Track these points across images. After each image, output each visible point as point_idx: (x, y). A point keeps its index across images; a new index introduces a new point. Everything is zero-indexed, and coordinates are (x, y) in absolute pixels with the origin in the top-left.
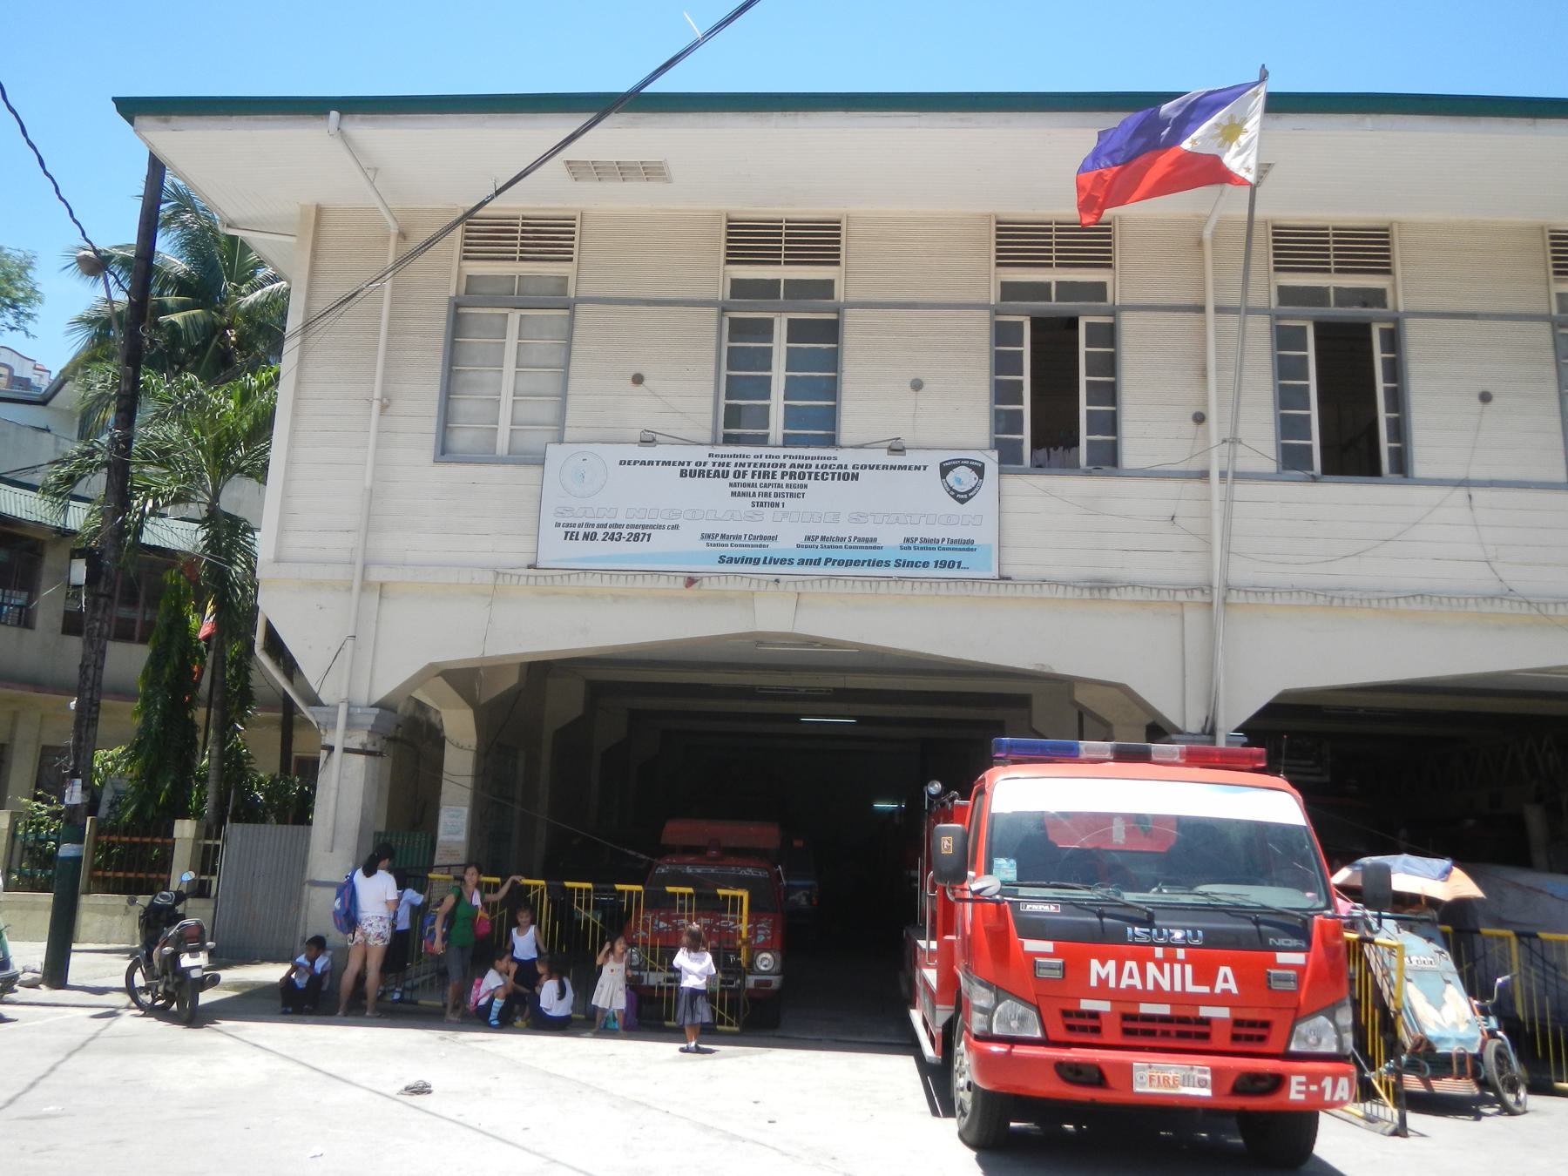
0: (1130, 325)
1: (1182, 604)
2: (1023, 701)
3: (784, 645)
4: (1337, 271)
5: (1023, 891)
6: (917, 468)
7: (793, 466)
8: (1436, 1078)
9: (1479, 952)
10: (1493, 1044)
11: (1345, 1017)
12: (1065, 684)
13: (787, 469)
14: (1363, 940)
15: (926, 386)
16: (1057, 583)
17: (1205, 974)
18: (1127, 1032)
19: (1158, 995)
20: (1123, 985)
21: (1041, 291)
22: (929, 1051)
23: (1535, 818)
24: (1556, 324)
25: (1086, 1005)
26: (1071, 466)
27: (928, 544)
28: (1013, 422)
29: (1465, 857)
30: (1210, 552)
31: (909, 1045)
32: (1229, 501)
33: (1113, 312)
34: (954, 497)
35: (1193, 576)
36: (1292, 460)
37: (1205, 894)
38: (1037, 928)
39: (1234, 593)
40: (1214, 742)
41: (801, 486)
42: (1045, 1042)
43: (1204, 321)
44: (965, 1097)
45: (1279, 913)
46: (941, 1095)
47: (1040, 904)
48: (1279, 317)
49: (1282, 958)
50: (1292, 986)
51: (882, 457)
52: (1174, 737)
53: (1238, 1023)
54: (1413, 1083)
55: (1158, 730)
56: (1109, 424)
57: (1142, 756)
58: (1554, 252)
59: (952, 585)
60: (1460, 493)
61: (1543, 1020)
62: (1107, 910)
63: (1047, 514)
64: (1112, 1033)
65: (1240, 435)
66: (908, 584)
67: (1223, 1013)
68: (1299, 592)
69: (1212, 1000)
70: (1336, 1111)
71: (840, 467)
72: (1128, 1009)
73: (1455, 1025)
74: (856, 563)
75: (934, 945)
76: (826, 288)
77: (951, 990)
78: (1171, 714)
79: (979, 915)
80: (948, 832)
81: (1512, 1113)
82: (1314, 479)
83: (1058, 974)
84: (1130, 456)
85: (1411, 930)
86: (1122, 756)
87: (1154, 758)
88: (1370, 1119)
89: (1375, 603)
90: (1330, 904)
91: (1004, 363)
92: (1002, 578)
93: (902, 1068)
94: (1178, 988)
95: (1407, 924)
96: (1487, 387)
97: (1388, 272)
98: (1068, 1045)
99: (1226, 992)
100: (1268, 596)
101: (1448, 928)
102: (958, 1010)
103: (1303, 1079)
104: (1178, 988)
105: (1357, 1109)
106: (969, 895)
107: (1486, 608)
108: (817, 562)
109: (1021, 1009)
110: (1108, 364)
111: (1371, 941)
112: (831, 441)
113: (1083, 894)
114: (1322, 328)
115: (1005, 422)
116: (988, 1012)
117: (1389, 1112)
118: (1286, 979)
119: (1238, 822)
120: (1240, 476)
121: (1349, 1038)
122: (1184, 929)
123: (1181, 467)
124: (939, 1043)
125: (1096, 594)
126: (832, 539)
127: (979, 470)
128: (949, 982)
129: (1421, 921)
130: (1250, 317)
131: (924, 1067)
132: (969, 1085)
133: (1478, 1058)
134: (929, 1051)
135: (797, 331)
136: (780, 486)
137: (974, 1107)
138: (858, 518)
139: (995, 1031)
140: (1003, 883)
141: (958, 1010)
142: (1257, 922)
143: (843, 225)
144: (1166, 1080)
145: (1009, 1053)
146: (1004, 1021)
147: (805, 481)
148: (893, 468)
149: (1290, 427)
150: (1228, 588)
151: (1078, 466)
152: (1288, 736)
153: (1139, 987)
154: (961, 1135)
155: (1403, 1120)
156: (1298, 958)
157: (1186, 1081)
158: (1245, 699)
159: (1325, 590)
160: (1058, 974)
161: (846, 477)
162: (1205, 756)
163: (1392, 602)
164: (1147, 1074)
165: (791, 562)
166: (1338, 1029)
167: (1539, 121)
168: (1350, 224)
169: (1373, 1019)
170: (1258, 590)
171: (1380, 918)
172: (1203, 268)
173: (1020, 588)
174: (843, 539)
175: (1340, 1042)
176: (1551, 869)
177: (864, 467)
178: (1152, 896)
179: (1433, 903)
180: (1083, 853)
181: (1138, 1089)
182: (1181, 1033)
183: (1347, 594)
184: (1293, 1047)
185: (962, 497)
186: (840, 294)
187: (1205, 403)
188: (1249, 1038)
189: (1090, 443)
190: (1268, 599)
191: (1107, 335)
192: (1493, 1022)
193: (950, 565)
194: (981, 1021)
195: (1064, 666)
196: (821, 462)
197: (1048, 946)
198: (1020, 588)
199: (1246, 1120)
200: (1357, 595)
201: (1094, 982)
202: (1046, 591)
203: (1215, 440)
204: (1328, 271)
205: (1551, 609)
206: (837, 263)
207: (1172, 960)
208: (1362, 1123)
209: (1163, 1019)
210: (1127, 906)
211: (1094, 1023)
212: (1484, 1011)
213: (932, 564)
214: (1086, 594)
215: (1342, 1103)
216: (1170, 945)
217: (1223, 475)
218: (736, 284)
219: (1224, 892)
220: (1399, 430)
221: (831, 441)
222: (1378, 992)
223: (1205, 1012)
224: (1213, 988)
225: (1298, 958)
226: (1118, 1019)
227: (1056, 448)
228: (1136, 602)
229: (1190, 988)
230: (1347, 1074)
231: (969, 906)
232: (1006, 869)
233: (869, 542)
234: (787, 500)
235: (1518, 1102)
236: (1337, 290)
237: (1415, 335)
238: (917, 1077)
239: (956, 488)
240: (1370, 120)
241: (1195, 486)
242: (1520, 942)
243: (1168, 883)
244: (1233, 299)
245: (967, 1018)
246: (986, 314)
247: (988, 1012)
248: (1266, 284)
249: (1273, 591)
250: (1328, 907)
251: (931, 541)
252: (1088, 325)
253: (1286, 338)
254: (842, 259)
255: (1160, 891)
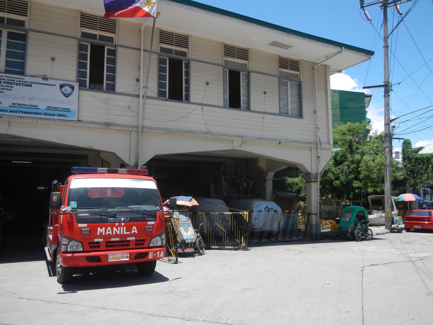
0: (120, 51)
1: (131, 131)
2: (85, 157)
3: (9, 138)
4: (175, 45)
5: (79, 210)
6: (52, 85)
7: (8, 80)
8: (185, 249)
9: (197, 218)
10: (199, 239)
11: (164, 236)
12: (97, 152)
13: (6, 81)
14: (170, 217)
15: (56, 60)
16: (95, 123)
17: (129, 229)
18: (107, 246)
19: (116, 236)
20: (107, 234)
21: (94, 36)
22: (49, 258)
23: (212, 186)
24: (279, 78)
25: (96, 240)
26: (100, 90)
27: (55, 109)
28: (84, 75)
29: (196, 196)
30: (139, 117)
31: (44, 258)
32: (144, 104)
33: (115, 46)
34: (64, 95)
35: (134, 123)
36: (161, 94)
37: (130, 208)
38: (82, 220)
39: (144, 129)
40: (137, 168)
41: (11, 87)
42: (83, 252)
43: (140, 53)
44: (60, 270)
45: (149, 212)
46: (52, 271)
47: (84, 213)
48: (160, 55)
49: (149, 223)
50: (151, 230)
51: (40, 80)
52: (127, 167)
53: (137, 240)
54: (180, 251)
55: (123, 165)
56: (113, 79)
57: (116, 172)
58: (27, 11)
59: (63, 122)
60: (201, 107)
61: (209, 233)
62: (103, 214)
63: (92, 104)
64: (103, 247)
65: (149, 86)
66: (48, 121)
67: (133, 238)
68: (161, 129)
69: (131, 235)
70: (161, 259)
71: (25, 82)
72: (108, 240)
73: (190, 236)
74: (30, 113)
75: (51, 228)
76: (22, 23)
77: (56, 241)
78: (126, 161)
79: (65, 218)
80: (55, 195)
81: (201, 255)
82: (166, 100)
83: (88, 232)
84: (119, 88)
85: (182, 214)
86: (110, 172)
87: (119, 172)
88: (169, 260)
89: (179, 133)
90: (162, 209)
91: (82, 57)
92: (78, 121)
93: (42, 265)
94: (122, 233)
95: (181, 213)
96: (208, 81)
97: (187, 48)
98: (90, 252)
99: (134, 233)
100: (153, 130)
101: (191, 213)
102: (58, 246)
103: (152, 253)
104: (122, 233)
105: (166, 259)
106: (62, 213)
107: (204, 136)
108: (16, 112)
109: (77, 243)
110: (113, 61)
111: (172, 217)
112: (22, 73)
113: (97, 210)
114: (92, 46)
115: (81, 75)
116: (67, 245)
117: (174, 258)
118: (150, 228)
119: (141, 189)
120: (148, 97)
121: (164, 241)
122: (124, 218)
123: (132, 93)
124: (52, 256)
125: (107, 127)
126: (22, 105)
127: (73, 88)
128: (56, 238)
129: (184, 212)
130: (152, 54)
131: (48, 263)
132: (61, 266)
133: (195, 243)
134: (49, 258)
135: (10, 35)
136: (3, 86)
137: (62, 272)
138: (31, 99)
139: (69, 250)
140: (72, 208)
141: (58, 246)
142: (143, 215)
143: (29, 3)
144: (117, 257)
145: (72, 256)
146: (72, 247)
147: (13, 85)
148: (44, 84)
149: (161, 85)
150: (143, 127)
151: (103, 90)
152: (157, 167)
153: (111, 234)
154: (58, 281)
155: (177, 259)
156: (153, 223)
157: (123, 257)
158: (146, 156)
159: (167, 129)
160: (88, 232)
161: (27, 85)
162: (134, 171)
163: (183, 133)
164: (112, 257)
165: (7, 111)
166: (162, 240)
167: (224, 16)
168: (180, 33)
169: (171, 236)
170: (151, 128)
171: (173, 212)
172: (141, 39)
173: (84, 124)
174: (26, 105)
175: (162, 243)
176: (215, 198)
177: (34, 83)
178: (116, 209)
179: (187, 207)
180: (98, 199)
181: (109, 261)
182: (122, 244)
183: (173, 130)
184: (150, 245)
185: (67, 96)
186: (27, 26)
187: (140, 76)
188: (140, 244)
189: (107, 83)
190: (153, 131)
191: (113, 53)
192: (199, 234)
193: (62, 116)
194: (64, 248)
195: (97, 146)
196: (18, 80)
197: (85, 225)
198: (84, 124)
199: (138, 264)
200: (175, 131)
201: (98, 234)
202: (92, 125)
203: (141, 87)
204: (173, 45)
205: (218, 136)
206: (26, 16)
207: (120, 226)
208: (168, 262)
209: (117, 242)
210: (109, 212)
211: (98, 245)
212: (197, 232)
213: (56, 115)
214: (104, 127)
215: (162, 257)
216: (120, 222)
217: (143, 96)
218: (161, 48)
219: (135, 207)
220: (188, 89)
221: (22, 73)
222: (173, 228)
223: (128, 239)
224: (131, 232)
225: (153, 223)
226: (105, 243)
227: (97, 84)
228: (118, 130)
229: (125, 233)
230: (163, 250)
231: (62, 216)
232: (74, 204)
233: (35, 107)
234: (6, 91)
235: (203, 252)
236: (8, 19)
237: (193, 65)
238: (46, 266)
239: (65, 92)
240: (355, 52)
241: (135, 99)
242: (206, 215)
243: (120, 206)
244: (148, 48)
245: (61, 248)
246: (76, 41)
247: (67, 245)
248: (157, 46)
249: (155, 129)
250: (161, 210)
251: (56, 108)
252: (108, 49)
253: (161, 61)
254: (28, 15)
255: (118, 208)
